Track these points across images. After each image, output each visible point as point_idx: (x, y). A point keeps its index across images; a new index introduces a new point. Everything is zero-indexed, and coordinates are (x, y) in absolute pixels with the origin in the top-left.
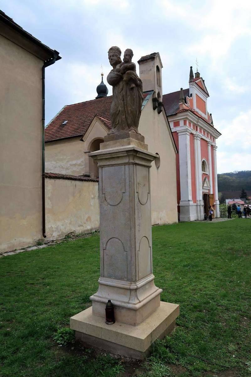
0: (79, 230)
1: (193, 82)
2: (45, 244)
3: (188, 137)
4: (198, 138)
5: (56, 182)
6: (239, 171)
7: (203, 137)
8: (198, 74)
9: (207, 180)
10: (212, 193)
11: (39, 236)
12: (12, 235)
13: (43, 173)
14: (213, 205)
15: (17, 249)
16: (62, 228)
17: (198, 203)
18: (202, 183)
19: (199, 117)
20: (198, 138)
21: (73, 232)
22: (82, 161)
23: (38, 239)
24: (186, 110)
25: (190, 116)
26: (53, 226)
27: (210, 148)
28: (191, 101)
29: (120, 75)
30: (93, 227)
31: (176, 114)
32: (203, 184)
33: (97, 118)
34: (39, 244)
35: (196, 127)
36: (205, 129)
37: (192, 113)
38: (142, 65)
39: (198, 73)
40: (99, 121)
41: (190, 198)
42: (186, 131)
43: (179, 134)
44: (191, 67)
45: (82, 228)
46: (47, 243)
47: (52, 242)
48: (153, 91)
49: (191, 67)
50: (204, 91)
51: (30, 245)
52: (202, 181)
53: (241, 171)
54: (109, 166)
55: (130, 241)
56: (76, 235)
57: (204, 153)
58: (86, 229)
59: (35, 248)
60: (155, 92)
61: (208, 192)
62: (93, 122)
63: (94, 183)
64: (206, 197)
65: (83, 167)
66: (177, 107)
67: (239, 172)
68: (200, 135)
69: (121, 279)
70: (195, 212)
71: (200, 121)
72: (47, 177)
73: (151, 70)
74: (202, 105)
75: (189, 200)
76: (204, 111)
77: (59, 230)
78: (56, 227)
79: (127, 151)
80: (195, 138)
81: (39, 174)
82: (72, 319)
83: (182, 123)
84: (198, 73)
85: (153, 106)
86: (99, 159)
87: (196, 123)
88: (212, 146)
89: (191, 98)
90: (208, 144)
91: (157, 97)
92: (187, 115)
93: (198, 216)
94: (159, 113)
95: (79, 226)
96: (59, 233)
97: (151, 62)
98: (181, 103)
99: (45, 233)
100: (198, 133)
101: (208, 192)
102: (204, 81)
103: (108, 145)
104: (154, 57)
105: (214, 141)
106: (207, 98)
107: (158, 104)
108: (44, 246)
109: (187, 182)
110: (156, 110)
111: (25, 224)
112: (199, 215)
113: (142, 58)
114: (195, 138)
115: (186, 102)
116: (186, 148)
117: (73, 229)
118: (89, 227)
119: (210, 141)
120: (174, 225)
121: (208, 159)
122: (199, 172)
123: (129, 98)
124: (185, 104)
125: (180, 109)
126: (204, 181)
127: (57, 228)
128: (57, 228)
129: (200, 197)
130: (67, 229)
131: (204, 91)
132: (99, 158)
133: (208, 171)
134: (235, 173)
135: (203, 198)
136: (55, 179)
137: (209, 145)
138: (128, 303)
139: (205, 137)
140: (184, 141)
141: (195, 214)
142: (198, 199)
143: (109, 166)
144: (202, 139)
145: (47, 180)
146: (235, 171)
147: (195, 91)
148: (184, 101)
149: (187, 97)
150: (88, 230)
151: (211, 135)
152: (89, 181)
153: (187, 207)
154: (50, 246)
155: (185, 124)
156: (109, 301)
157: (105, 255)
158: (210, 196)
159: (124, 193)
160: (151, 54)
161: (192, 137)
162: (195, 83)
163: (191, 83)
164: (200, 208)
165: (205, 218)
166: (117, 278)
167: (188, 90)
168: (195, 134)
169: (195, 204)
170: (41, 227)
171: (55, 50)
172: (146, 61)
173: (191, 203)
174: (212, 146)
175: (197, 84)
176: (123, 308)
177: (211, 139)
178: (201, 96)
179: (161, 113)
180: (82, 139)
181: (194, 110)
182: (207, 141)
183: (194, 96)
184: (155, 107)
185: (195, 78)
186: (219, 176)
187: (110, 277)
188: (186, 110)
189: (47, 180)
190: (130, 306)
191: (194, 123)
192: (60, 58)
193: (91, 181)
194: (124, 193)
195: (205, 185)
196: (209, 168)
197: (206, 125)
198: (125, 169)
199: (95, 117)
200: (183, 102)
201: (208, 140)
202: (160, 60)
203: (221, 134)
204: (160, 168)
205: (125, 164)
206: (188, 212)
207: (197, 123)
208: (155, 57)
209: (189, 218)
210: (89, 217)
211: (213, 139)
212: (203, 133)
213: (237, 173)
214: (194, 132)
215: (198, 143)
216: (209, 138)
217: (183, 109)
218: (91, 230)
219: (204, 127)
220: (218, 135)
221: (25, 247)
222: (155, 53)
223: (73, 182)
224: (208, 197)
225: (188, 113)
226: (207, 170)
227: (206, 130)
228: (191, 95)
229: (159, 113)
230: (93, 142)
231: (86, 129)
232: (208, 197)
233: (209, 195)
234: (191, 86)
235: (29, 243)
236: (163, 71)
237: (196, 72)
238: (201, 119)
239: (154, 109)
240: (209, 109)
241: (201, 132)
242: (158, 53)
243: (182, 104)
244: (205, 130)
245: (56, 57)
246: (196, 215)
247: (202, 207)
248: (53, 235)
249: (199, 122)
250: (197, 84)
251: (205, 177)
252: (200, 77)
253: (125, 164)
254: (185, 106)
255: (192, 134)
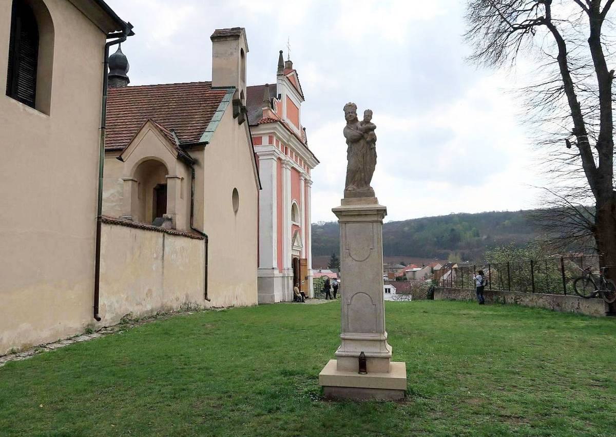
0: (137, 311)
1: (284, 75)
2: (97, 332)
3: (275, 164)
4: (288, 167)
5: (112, 229)
6: (327, 221)
7: (295, 164)
8: (290, 63)
9: (298, 235)
10: (304, 257)
11: (88, 318)
12: (48, 317)
13: (98, 214)
14: (306, 278)
15: (62, 339)
16: (116, 305)
17: (286, 272)
18: (291, 239)
19: (291, 133)
20: (288, 167)
21: (129, 314)
22: (112, 194)
23: (87, 323)
24: (275, 121)
25: (280, 131)
26: (106, 302)
27: (303, 182)
28: (280, 105)
29: (361, 134)
30: (154, 306)
31: (257, 125)
32: (293, 242)
33: (151, 125)
34: (89, 332)
35: (286, 148)
36: (293, 149)
37: (282, 126)
38: (217, 44)
39: (289, 61)
40: (156, 130)
41: (275, 265)
42: (272, 153)
43: (260, 158)
44: (281, 52)
45: (140, 307)
46: (98, 331)
47: (105, 329)
48: (234, 87)
49: (281, 52)
50: (298, 91)
51: (78, 333)
52: (291, 237)
53: (330, 222)
54: (354, 222)
55: (379, 294)
56: (133, 319)
57: (296, 193)
58: (146, 309)
59: (86, 338)
60: (237, 90)
61: (298, 254)
62: (144, 130)
63: (158, 233)
64: (296, 263)
65: (114, 204)
66: (257, 113)
67: (326, 223)
68: (291, 161)
69: (370, 331)
70: (280, 288)
71: (292, 139)
72: (107, 222)
73: (232, 54)
74: (294, 112)
75: (274, 267)
76: (297, 124)
77: (113, 309)
78: (109, 304)
79: (377, 210)
80: (284, 166)
81: (93, 216)
82: (321, 375)
83: (265, 140)
84: (289, 61)
85: (234, 112)
86: (344, 215)
87: (286, 142)
88: (306, 179)
89: (280, 101)
90: (300, 176)
91: (240, 98)
92: (275, 128)
93: (284, 295)
94: (240, 123)
95: (137, 305)
96: (113, 315)
97: (232, 41)
98: (266, 108)
99: (98, 313)
100: (288, 159)
101: (298, 254)
102: (297, 75)
103: (351, 201)
104: (239, 35)
105: (308, 172)
106: (301, 102)
107: (241, 109)
108: (95, 335)
109: (271, 237)
110: (237, 118)
111: (73, 297)
112: (286, 292)
113: (217, 31)
114: (284, 166)
115: (272, 108)
116: (272, 181)
117: (131, 309)
118: (149, 307)
119: (304, 172)
120: (254, 307)
121: (299, 203)
122: (288, 222)
123: (368, 157)
124: (271, 111)
125: (264, 118)
126: (294, 237)
127: (110, 306)
128: (116, 303)
129: (288, 264)
130: (122, 309)
131: (298, 91)
132: (344, 214)
133: (299, 220)
134: (320, 224)
135: (292, 265)
136: (112, 225)
137: (302, 178)
138: (380, 353)
139: (297, 166)
140: (268, 168)
141: (281, 292)
142: (285, 267)
143: (354, 222)
144: (293, 168)
145: (105, 228)
146: (321, 222)
147: (284, 90)
148: (270, 105)
149: (275, 98)
150: (147, 312)
151: (305, 162)
152: (153, 230)
153: (269, 279)
154: (104, 336)
155: (271, 142)
156: (362, 353)
157: (349, 310)
158: (301, 262)
159: (372, 249)
160: (233, 29)
161: (279, 164)
162: (287, 77)
163: (281, 78)
164: (288, 281)
165: (296, 299)
166: (363, 332)
167: (273, 88)
168: (301, 172)
169: (281, 275)
170: (92, 304)
171: (130, 22)
172: (224, 39)
173: (276, 272)
174: (306, 179)
175: (289, 80)
176: (374, 358)
177: (304, 168)
178: (294, 98)
179: (243, 124)
180: (120, 156)
181: (283, 120)
182: (299, 172)
183: (284, 98)
184: (236, 114)
185: (285, 68)
186: (314, 227)
187: (356, 331)
188: (275, 121)
189: (105, 228)
190: (383, 355)
191: (283, 142)
192: (132, 34)
193: (155, 231)
194: (372, 249)
195: (296, 244)
196: (301, 217)
197: (300, 147)
198: (373, 226)
199: (148, 123)
200: (269, 106)
201: (301, 170)
202: (245, 39)
203: (319, 162)
204: (238, 211)
205: (373, 222)
206: (271, 286)
207: (288, 141)
208: (240, 34)
209: (273, 297)
210: (150, 290)
211: (308, 169)
212: (291, 154)
213: (324, 224)
214: (283, 157)
215: (287, 174)
216: (303, 167)
217: (269, 119)
218: (152, 311)
219: (297, 150)
220: (315, 163)
221: (72, 336)
222: (239, 28)
223: (134, 231)
224: (298, 264)
225: (276, 126)
226: (298, 218)
227: (299, 154)
228: (280, 95)
229: (240, 123)
230: (141, 164)
231: (129, 141)
232: (298, 264)
233: (299, 260)
234: (280, 81)
235: (76, 330)
236: (248, 56)
237: (287, 60)
238: (293, 136)
239: (234, 117)
240: (303, 123)
241: (292, 156)
242: (243, 29)
243: (266, 110)
244: (297, 154)
245: (128, 32)
246: (281, 293)
247: (291, 279)
248: (106, 318)
249: (291, 141)
250: (289, 80)
251: (296, 229)
252: (293, 68)
253: (373, 222)
254: (271, 114)
255: (279, 159)
